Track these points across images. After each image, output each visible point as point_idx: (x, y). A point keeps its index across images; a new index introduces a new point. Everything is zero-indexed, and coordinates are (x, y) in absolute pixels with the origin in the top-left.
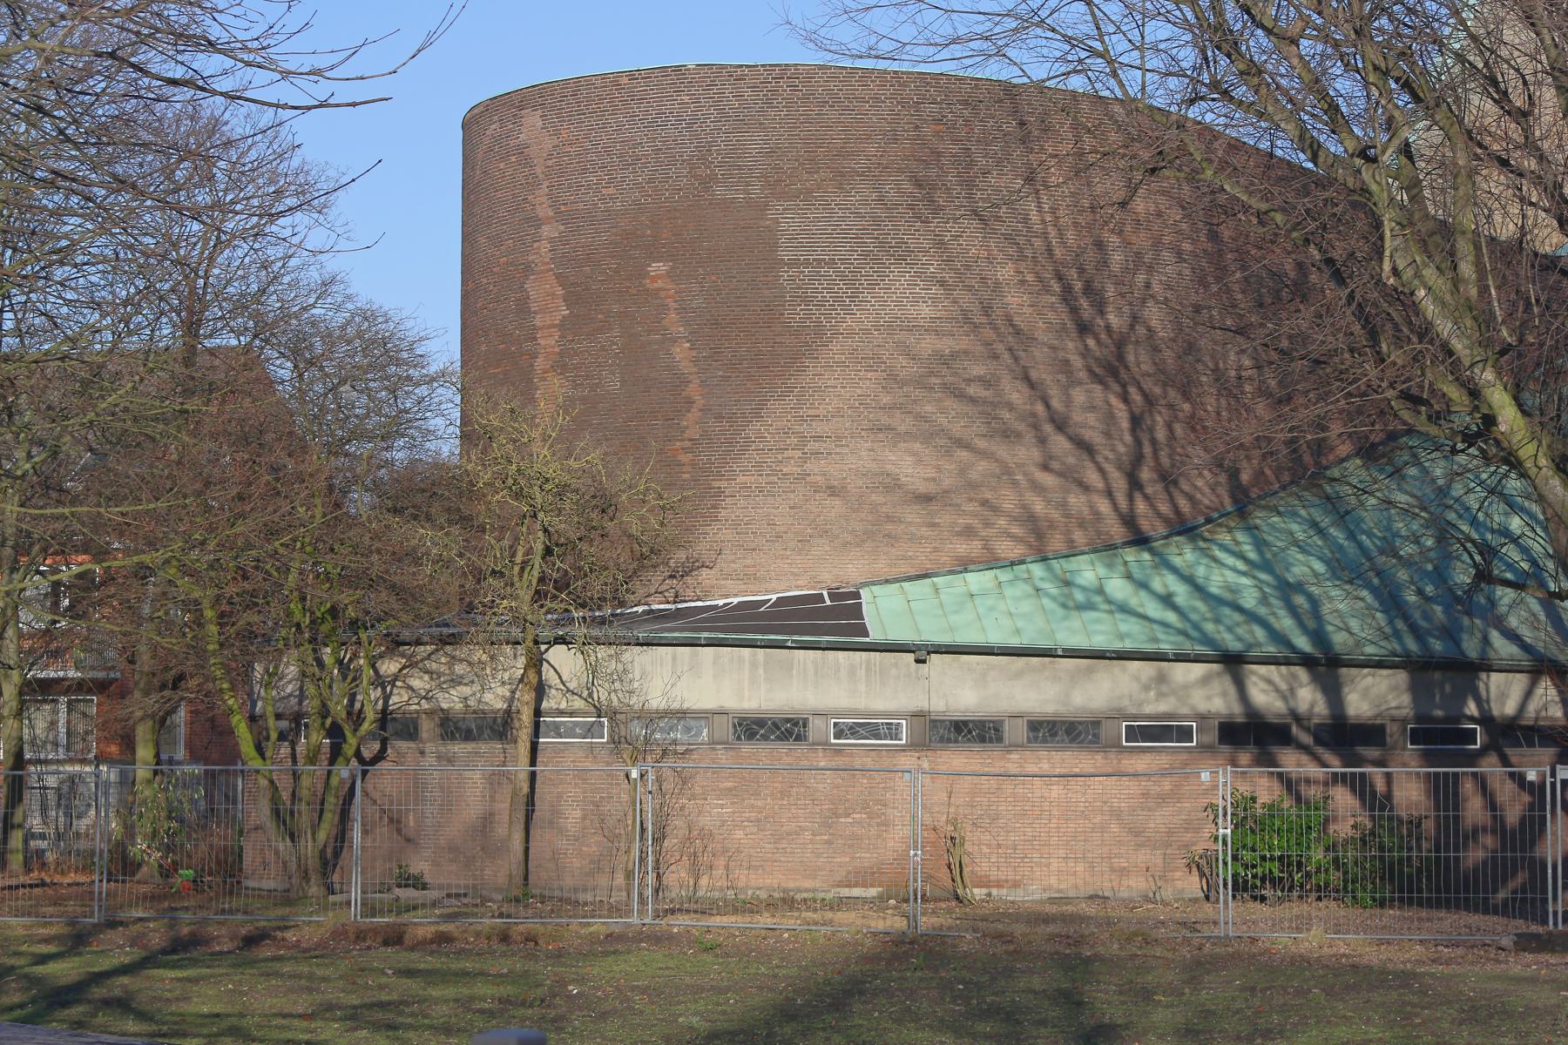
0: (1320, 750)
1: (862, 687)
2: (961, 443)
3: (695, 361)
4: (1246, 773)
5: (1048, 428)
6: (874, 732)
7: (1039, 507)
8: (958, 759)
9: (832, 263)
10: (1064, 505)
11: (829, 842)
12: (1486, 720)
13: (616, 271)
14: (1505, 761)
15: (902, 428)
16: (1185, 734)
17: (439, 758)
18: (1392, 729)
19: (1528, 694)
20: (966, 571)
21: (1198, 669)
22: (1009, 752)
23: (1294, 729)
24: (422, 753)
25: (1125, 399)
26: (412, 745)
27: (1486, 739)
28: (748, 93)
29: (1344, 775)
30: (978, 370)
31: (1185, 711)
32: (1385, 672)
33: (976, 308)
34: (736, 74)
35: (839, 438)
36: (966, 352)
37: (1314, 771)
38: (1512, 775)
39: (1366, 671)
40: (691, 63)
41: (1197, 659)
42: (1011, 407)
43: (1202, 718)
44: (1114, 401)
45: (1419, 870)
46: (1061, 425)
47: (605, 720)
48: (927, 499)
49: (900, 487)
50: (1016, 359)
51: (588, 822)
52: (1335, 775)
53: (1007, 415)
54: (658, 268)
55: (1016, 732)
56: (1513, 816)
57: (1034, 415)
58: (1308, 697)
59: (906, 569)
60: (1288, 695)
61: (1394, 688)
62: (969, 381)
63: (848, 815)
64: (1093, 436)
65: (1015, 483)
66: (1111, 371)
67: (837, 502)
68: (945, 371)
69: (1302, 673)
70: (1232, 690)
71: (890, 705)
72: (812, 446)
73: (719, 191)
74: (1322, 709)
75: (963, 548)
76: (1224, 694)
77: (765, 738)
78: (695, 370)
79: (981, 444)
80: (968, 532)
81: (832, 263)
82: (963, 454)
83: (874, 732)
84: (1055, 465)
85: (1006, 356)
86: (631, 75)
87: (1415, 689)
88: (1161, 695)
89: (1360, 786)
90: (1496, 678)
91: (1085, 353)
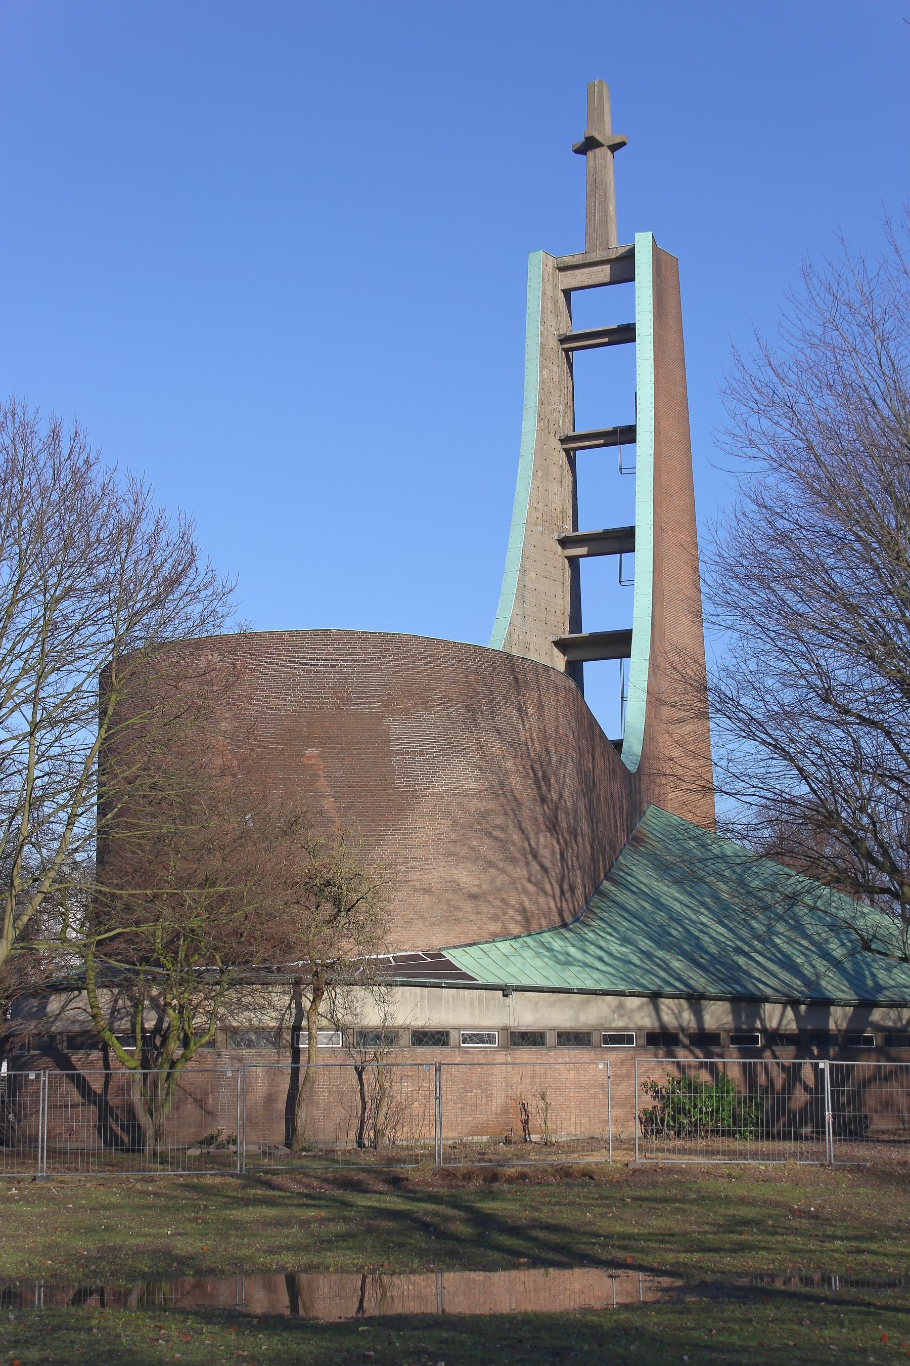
0: (693, 1048)
1: (477, 1012)
2: (491, 864)
3: (338, 810)
4: (661, 1062)
5: (530, 857)
6: (481, 1039)
7: (527, 903)
8: (525, 1055)
9: (421, 753)
10: (537, 903)
11: (462, 1108)
12: (764, 1031)
13: (281, 752)
14: (775, 1057)
15: (462, 854)
16: (630, 1039)
17: (232, 1058)
18: (723, 1036)
19: (782, 1015)
20: (494, 941)
21: (637, 1001)
22: (550, 1051)
23: (681, 1036)
24: (219, 1055)
25: (559, 842)
26: (211, 1050)
27: (764, 1041)
28: (370, 649)
29: (706, 1063)
30: (499, 821)
31: (632, 1026)
32: (720, 1003)
33: (496, 784)
34: (364, 637)
35: (427, 859)
36: (492, 810)
37: (692, 1060)
38: (778, 1064)
39: (712, 1002)
40: (334, 629)
41: (639, 995)
42: (514, 844)
43: (639, 1029)
44: (555, 843)
45: (778, 1120)
46: (535, 856)
47: (340, 1033)
48: (474, 897)
49: (460, 889)
50: (515, 815)
51: (332, 1099)
52: (701, 1062)
53: (512, 848)
54: (312, 751)
55: (551, 1038)
56: (779, 1083)
57: (524, 849)
58: (688, 1017)
59: (463, 940)
60: (678, 1016)
61: (724, 1012)
62: (494, 827)
63: (471, 1091)
64: (547, 863)
65: (516, 889)
66: (553, 826)
67: (427, 898)
68: (482, 821)
69: (684, 1003)
70: (653, 1013)
71: (486, 1023)
72: (413, 864)
73: (353, 707)
74: (693, 1024)
75: (493, 927)
76: (649, 1016)
77: (427, 1044)
78: (338, 815)
79: (501, 865)
80: (495, 918)
81: (421, 753)
82: (492, 871)
83: (481, 1039)
84: (533, 880)
85: (511, 813)
86: (291, 633)
87: (736, 1013)
88: (621, 1016)
89: (712, 1069)
90: (768, 1006)
91: (544, 814)
